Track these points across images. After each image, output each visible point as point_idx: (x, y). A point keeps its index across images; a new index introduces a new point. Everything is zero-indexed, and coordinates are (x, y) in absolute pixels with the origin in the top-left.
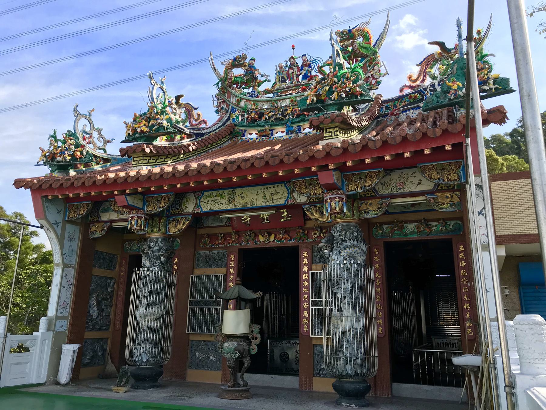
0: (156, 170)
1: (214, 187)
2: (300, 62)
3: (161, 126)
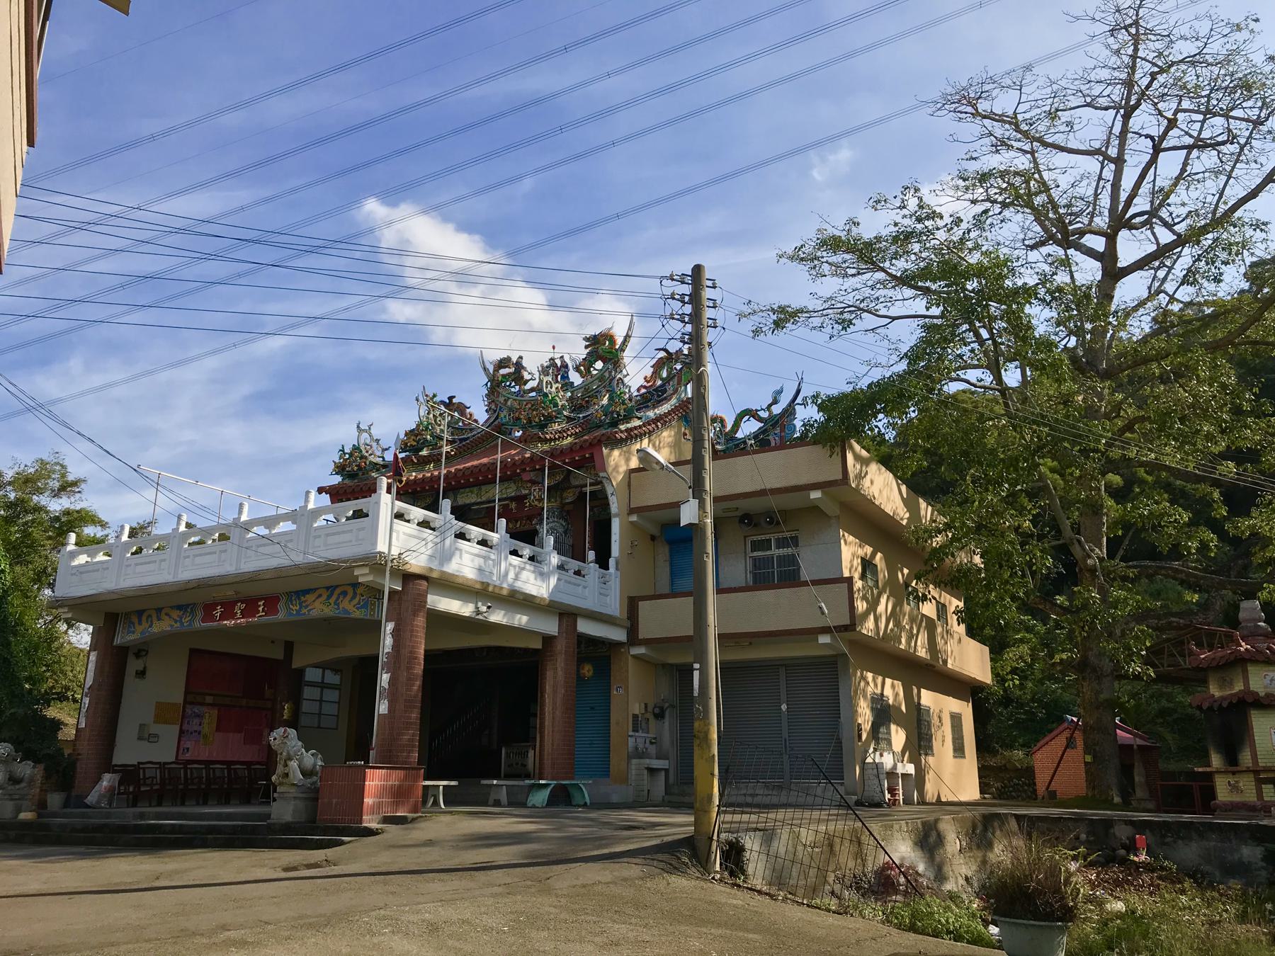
0: (420, 476)
1: (468, 485)
2: (558, 362)
3: (426, 440)
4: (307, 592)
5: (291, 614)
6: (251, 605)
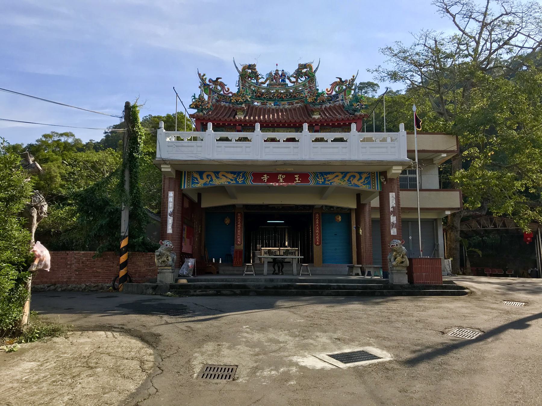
2: (280, 73)
4: (329, 173)
5: (318, 183)
6: (237, 173)
